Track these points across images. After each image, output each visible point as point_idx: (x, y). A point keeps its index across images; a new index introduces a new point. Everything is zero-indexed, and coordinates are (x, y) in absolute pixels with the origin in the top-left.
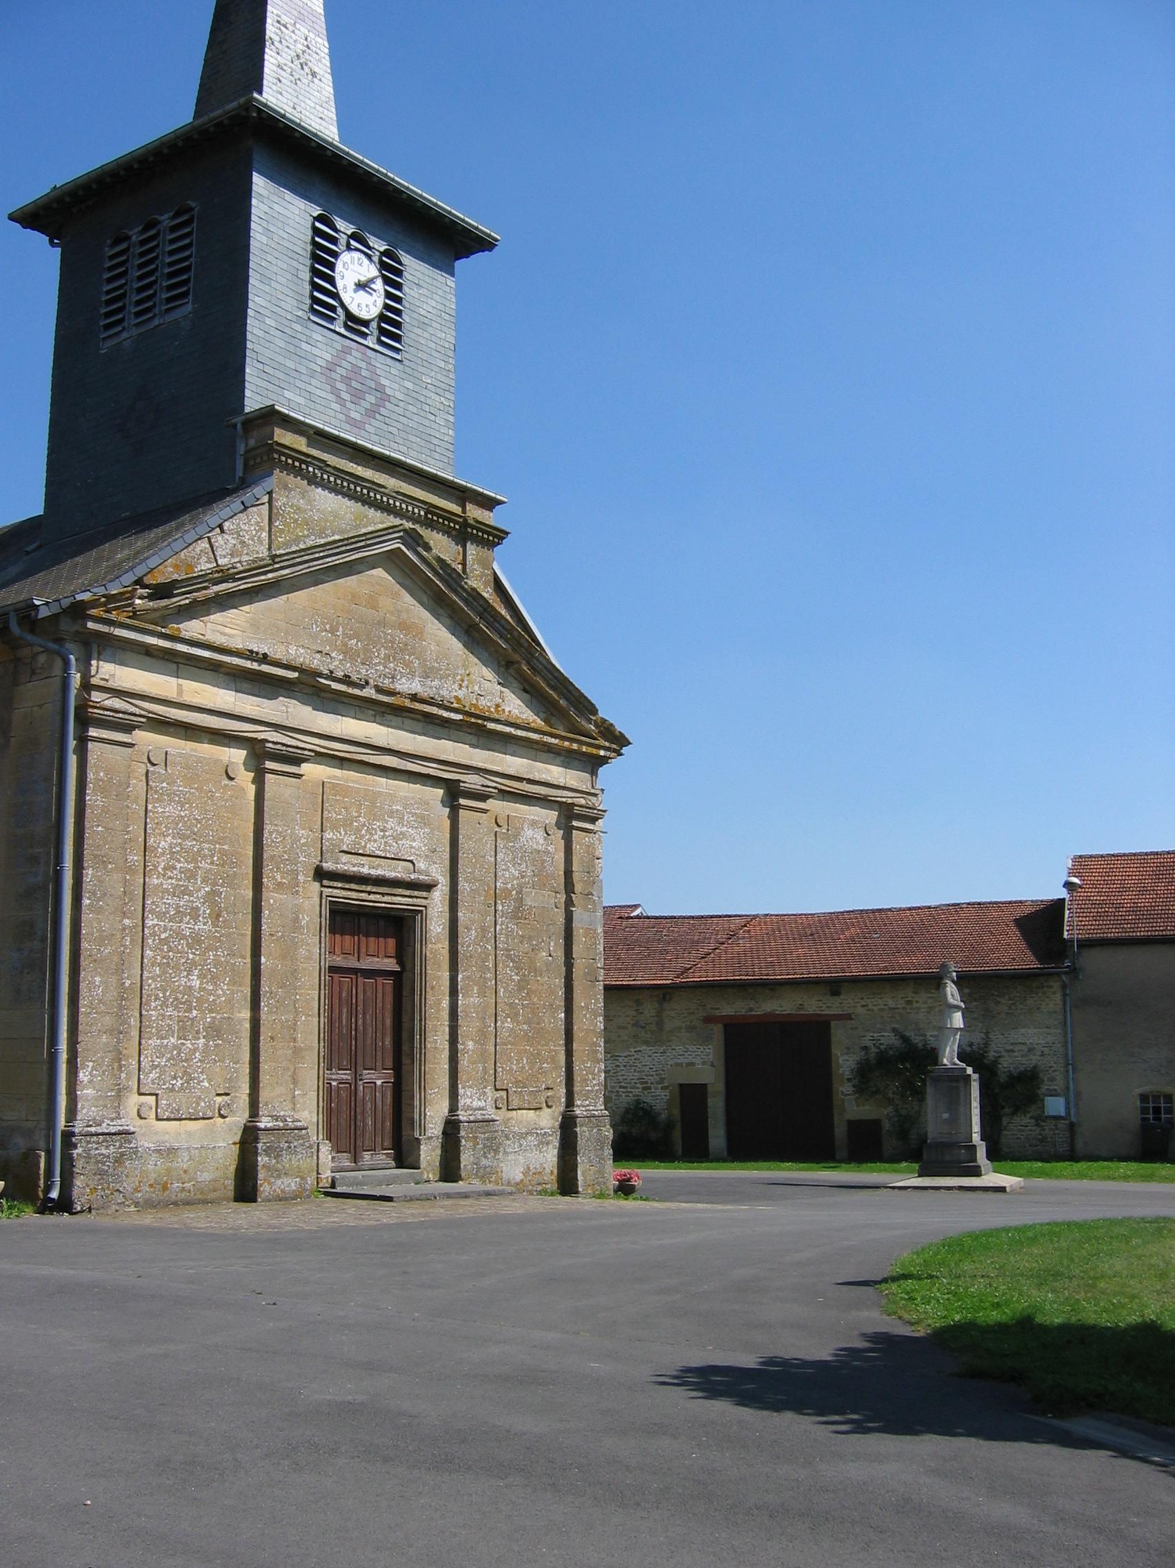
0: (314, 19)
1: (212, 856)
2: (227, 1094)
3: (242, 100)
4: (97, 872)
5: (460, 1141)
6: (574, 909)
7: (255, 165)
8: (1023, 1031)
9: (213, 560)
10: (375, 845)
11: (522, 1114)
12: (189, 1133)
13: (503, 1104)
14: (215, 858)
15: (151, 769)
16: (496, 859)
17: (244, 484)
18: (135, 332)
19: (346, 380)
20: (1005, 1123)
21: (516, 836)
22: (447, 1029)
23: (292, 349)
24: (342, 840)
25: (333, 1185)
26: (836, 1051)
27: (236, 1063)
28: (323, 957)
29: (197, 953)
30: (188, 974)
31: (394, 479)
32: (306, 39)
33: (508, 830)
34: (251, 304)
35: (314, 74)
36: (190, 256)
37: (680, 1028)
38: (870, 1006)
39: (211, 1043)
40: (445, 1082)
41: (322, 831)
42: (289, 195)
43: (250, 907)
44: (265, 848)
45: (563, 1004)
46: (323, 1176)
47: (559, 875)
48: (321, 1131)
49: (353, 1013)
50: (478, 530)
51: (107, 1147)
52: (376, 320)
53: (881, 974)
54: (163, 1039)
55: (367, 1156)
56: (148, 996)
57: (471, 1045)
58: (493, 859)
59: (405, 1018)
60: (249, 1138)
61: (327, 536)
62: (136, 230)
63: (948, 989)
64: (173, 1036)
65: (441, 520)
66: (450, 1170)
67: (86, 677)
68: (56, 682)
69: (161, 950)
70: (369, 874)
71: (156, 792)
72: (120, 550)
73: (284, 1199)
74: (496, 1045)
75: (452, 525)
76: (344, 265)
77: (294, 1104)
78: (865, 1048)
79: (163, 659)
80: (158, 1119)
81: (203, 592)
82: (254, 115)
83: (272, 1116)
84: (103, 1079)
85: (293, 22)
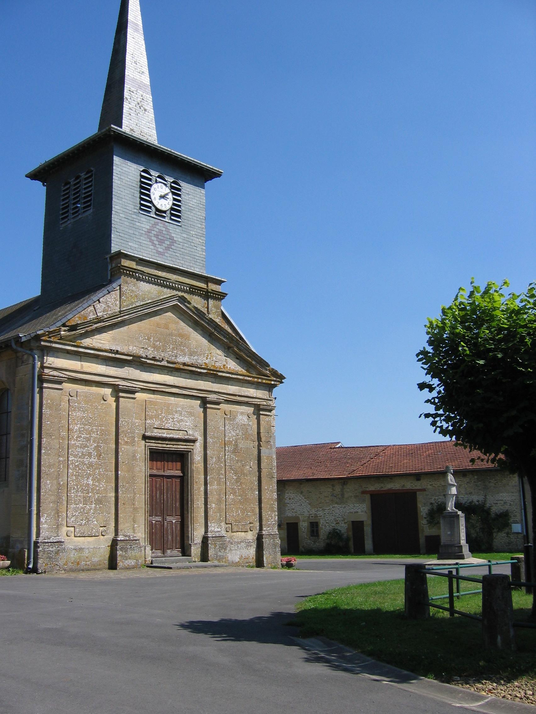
0: (146, 87)
1: (97, 432)
2: (105, 527)
3: (107, 128)
4: (48, 439)
5: (208, 545)
6: (261, 448)
7: (115, 153)
8: (501, 494)
9: (96, 314)
10: (169, 425)
11: (239, 534)
12: (88, 542)
13: (229, 530)
14: (99, 433)
15: (71, 398)
16: (225, 429)
17: (110, 282)
18: (72, 221)
19: (156, 236)
20: (494, 536)
21: (234, 419)
22: (203, 499)
23: (132, 225)
24: (155, 423)
25: (152, 563)
26: (419, 505)
27: (109, 514)
28: (146, 471)
29: (91, 470)
30: (87, 479)
31: (176, 276)
32: (142, 96)
33: (230, 416)
34: (113, 209)
35: (145, 110)
36: (92, 190)
37: (351, 496)
38: (434, 485)
39: (98, 506)
40: (203, 521)
41: (145, 420)
42: (129, 163)
43: (114, 451)
44: (120, 428)
45: (257, 488)
46: (147, 559)
47: (255, 434)
48: (146, 541)
49: (162, 493)
50: (213, 294)
51: (52, 548)
52: (169, 210)
53: (437, 471)
54: (77, 505)
55: (169, 551)
56: (70, 488)
57: (214, 505)
58: (224, 429)
59: (185, 495)
60: (115, 543)
61: (145, 301)
62: (73, 180)
63: (449, 478)
64: (81, 504)
65: (196, 291)
66: (204, 557)
67: (42, 363)
68: (30, 366)
69: (76, 470)
70: (166, 437)
71: (73, 407)
72: (60, 311)
73: (128, 568)
74: (226, 505)
75: (202, 292)
76: (154, 189)
77: (134, 530)
78: (431, 504)
79: (74, 354)
80: (75, 537)
81: (90, 327)
82: (112, 133)
83: (124, 535)
84: (51, 521)
85: (136, 90)
